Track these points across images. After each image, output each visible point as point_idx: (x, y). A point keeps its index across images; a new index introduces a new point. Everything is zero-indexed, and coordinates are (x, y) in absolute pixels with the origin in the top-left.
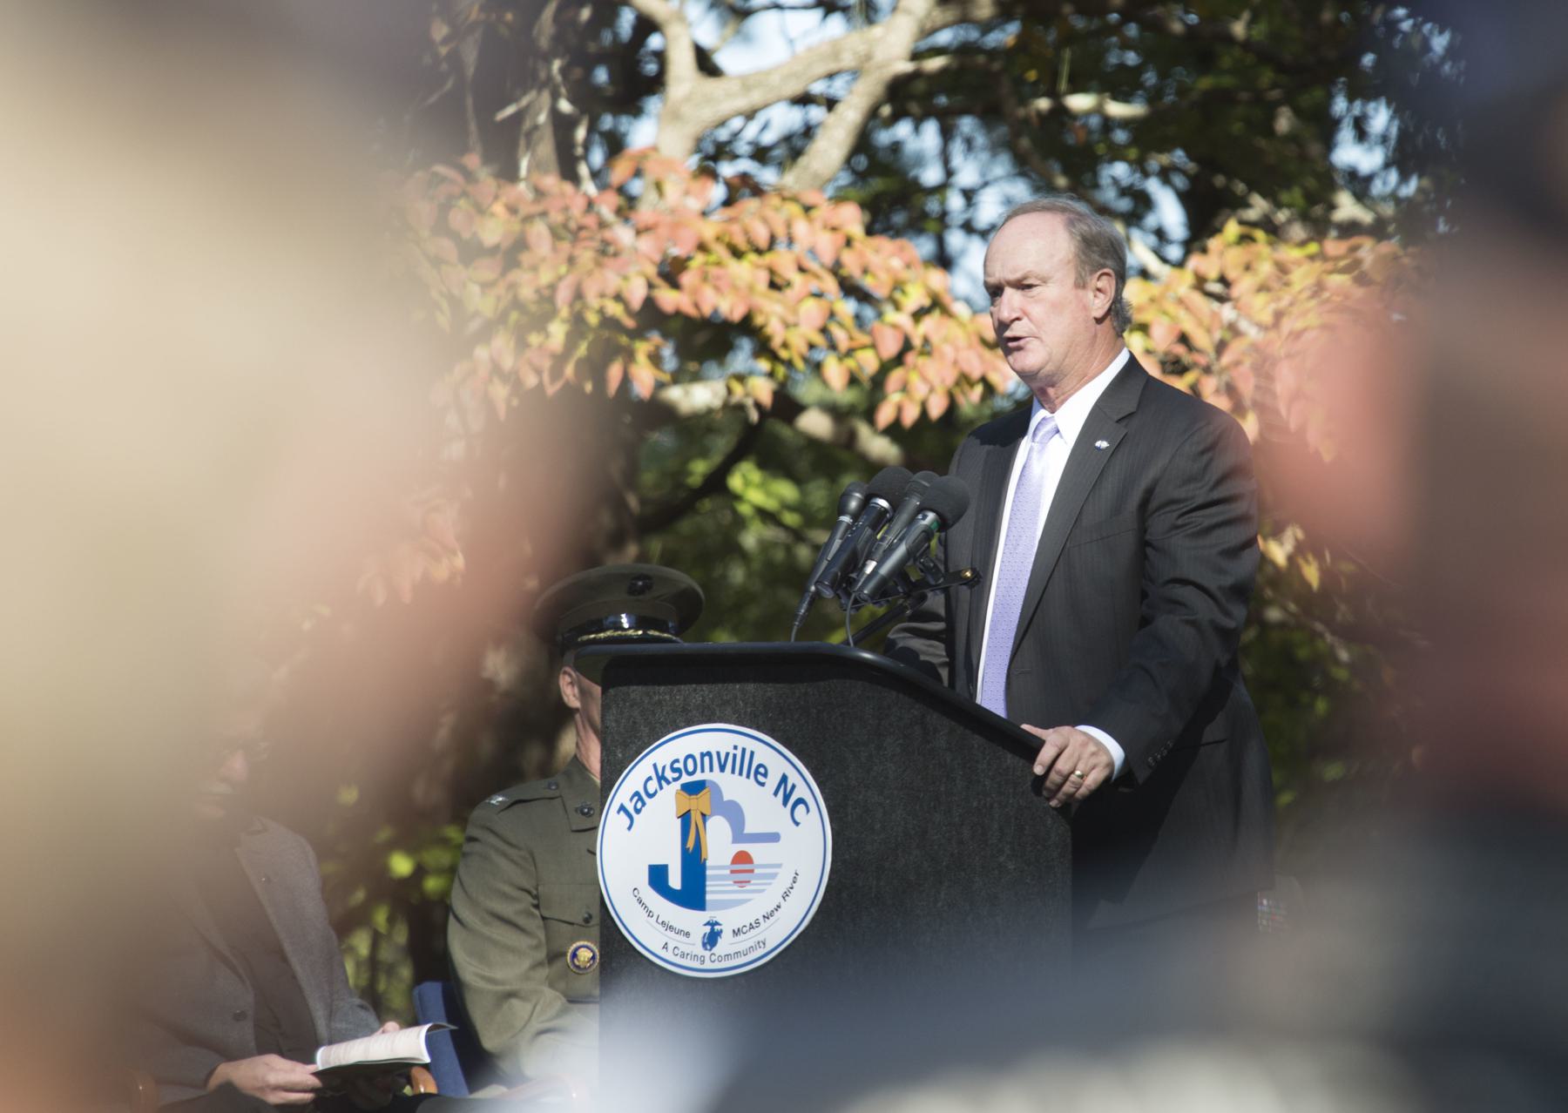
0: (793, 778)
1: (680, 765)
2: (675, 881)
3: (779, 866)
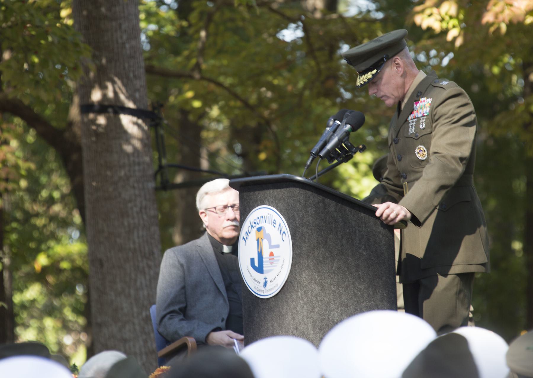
0: (282, 225)
1: (256, 221)
2: (256, 264)
3: (279, 257)
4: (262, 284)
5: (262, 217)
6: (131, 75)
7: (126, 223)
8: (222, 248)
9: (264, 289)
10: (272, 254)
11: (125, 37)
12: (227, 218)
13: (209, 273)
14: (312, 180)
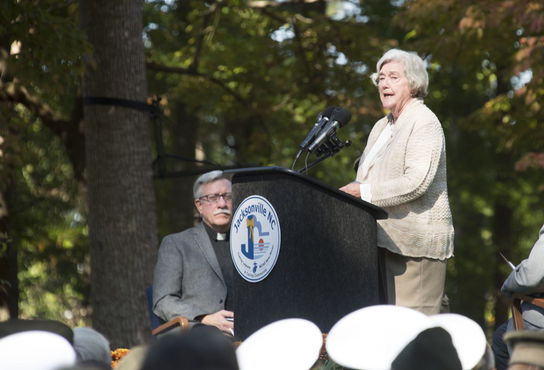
0: (272, 214)
1: (247, 210)
3: (269, 243)
4: (252, 269)
6: (133, 70)
7: (125, 209)
8: (216, 235)
9: (254, 274)
10: (261, 241)
12: (218, 206)
13: (206, 259)
14: (300, 172)
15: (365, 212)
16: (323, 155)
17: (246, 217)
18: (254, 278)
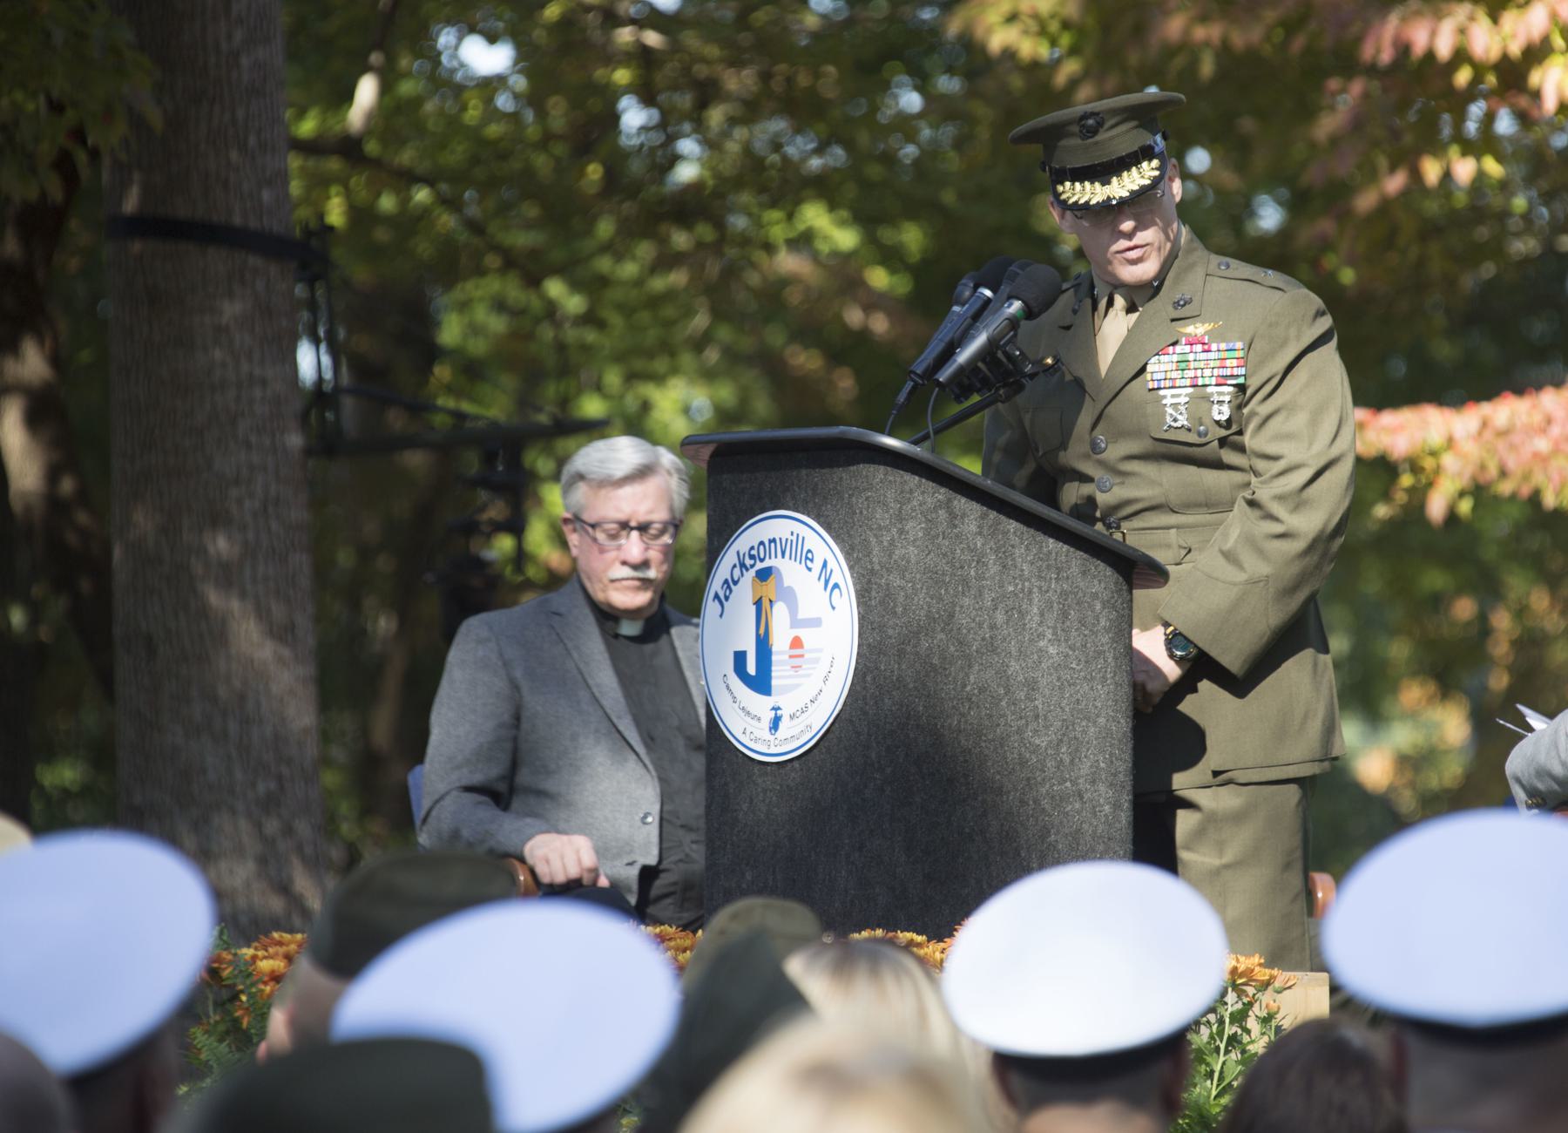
0: (832, 564)
2: (751, 669)
3: (820, 650)
4: (766, 723)
5: (774, 540)
6: (252, 140)
10: (797, 643)
11: (239, 35)
15: (1102, 566)
16: (976, 398)
17: (752, 572)
18: (773, 750)
